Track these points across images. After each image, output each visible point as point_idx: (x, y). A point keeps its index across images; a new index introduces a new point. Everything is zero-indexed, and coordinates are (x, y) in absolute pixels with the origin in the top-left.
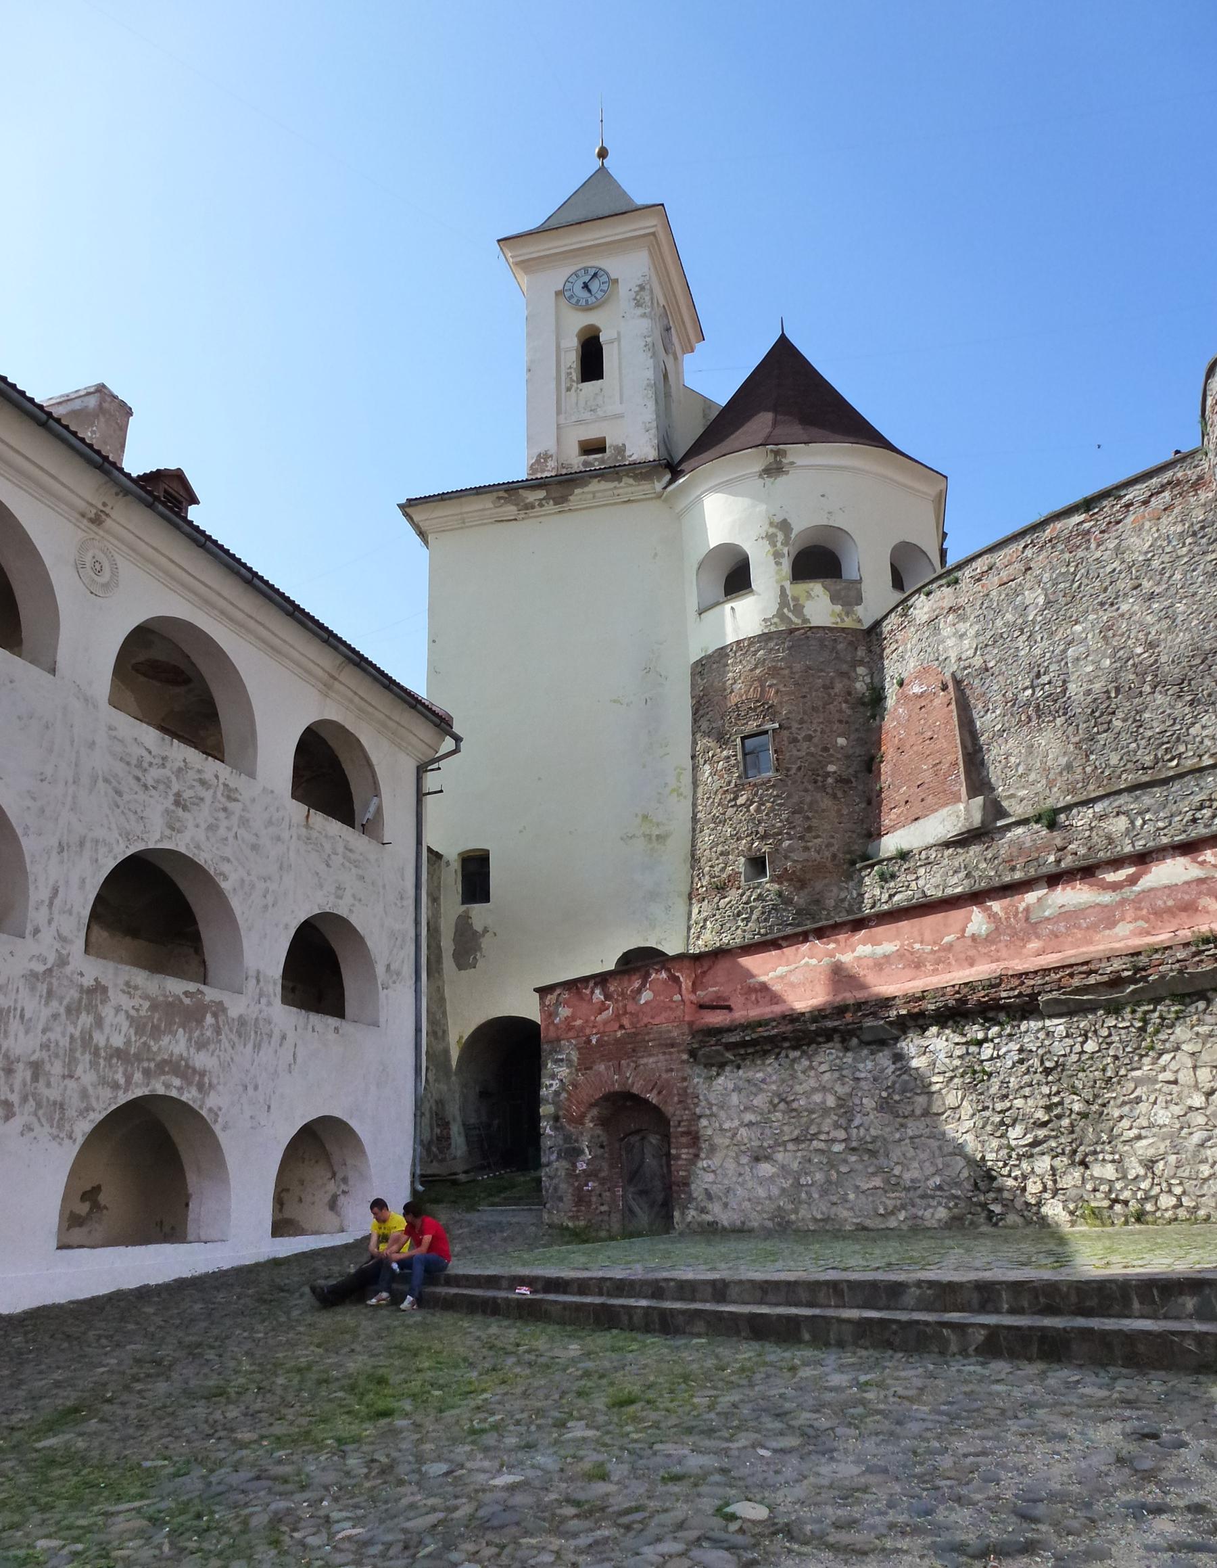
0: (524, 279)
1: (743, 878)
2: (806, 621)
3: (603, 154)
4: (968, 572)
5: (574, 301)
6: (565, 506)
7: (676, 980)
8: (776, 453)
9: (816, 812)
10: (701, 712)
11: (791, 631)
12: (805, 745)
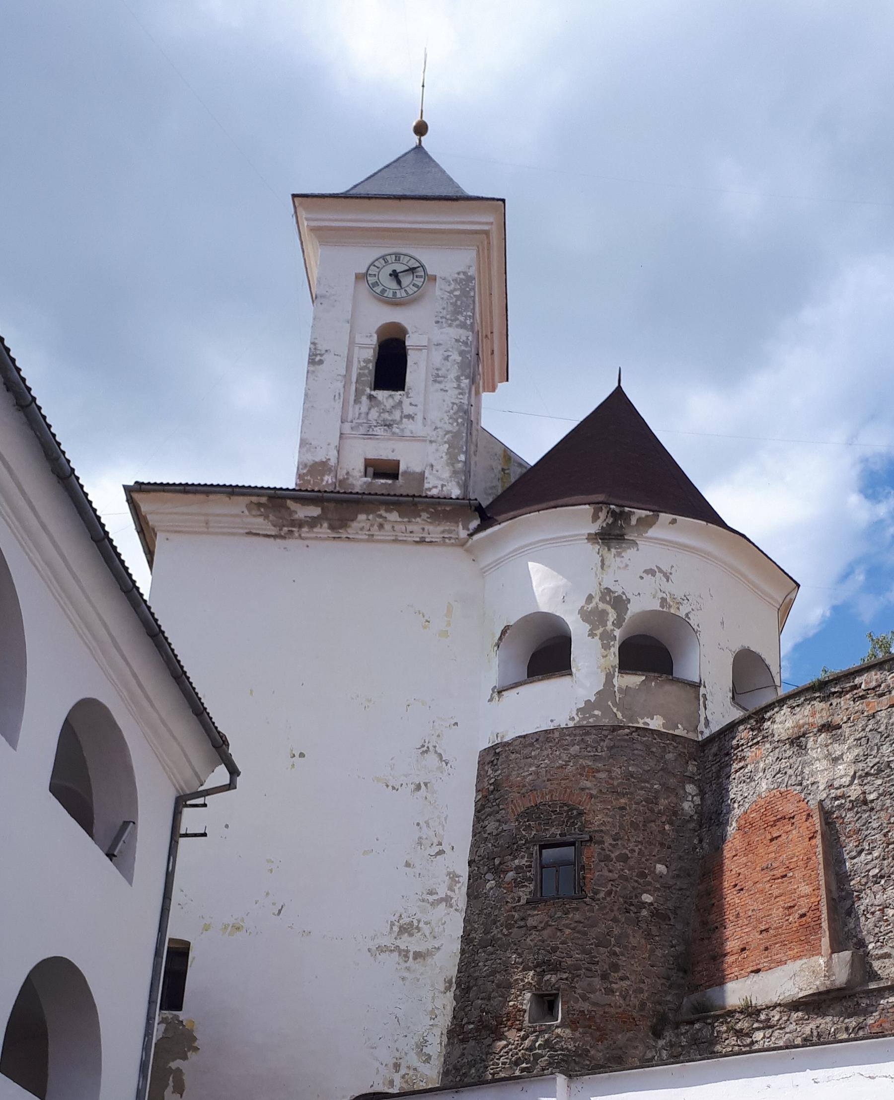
0: (315, 252)
1: (527, 1018)
3: (421, 129)
5: (378, 289)
9: (626, 947)
11: (614, 729)
12: (619, 866)
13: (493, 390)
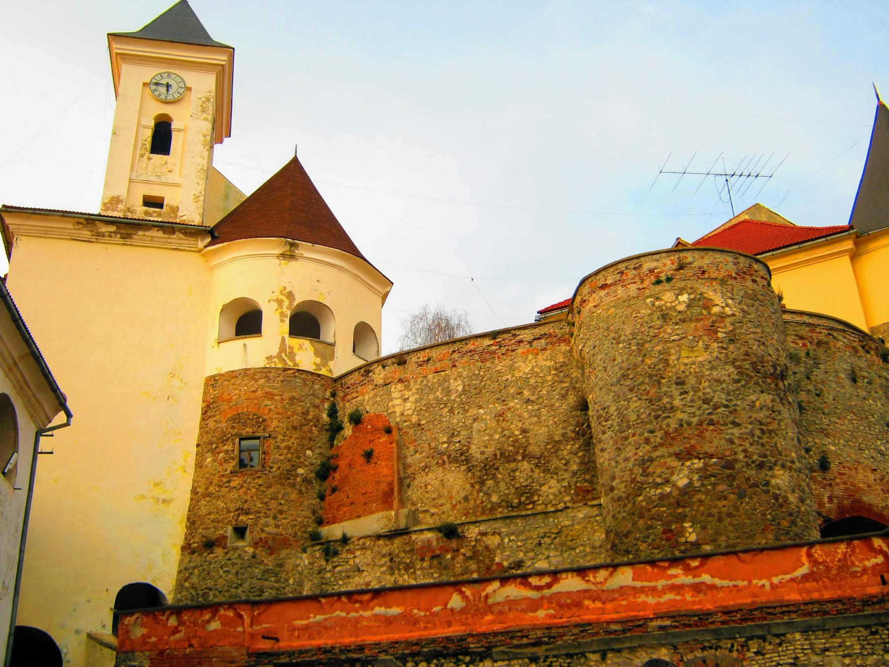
2: (295, 364)
4: (414, 358)
5: (157, 94)
6: (129, 241)
7: (240, 617)
8: (292, 245)
10: (209, 414)
11: (285, 370)
13: (221, 142)
